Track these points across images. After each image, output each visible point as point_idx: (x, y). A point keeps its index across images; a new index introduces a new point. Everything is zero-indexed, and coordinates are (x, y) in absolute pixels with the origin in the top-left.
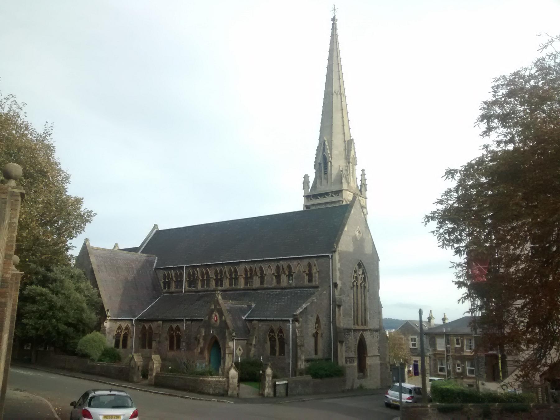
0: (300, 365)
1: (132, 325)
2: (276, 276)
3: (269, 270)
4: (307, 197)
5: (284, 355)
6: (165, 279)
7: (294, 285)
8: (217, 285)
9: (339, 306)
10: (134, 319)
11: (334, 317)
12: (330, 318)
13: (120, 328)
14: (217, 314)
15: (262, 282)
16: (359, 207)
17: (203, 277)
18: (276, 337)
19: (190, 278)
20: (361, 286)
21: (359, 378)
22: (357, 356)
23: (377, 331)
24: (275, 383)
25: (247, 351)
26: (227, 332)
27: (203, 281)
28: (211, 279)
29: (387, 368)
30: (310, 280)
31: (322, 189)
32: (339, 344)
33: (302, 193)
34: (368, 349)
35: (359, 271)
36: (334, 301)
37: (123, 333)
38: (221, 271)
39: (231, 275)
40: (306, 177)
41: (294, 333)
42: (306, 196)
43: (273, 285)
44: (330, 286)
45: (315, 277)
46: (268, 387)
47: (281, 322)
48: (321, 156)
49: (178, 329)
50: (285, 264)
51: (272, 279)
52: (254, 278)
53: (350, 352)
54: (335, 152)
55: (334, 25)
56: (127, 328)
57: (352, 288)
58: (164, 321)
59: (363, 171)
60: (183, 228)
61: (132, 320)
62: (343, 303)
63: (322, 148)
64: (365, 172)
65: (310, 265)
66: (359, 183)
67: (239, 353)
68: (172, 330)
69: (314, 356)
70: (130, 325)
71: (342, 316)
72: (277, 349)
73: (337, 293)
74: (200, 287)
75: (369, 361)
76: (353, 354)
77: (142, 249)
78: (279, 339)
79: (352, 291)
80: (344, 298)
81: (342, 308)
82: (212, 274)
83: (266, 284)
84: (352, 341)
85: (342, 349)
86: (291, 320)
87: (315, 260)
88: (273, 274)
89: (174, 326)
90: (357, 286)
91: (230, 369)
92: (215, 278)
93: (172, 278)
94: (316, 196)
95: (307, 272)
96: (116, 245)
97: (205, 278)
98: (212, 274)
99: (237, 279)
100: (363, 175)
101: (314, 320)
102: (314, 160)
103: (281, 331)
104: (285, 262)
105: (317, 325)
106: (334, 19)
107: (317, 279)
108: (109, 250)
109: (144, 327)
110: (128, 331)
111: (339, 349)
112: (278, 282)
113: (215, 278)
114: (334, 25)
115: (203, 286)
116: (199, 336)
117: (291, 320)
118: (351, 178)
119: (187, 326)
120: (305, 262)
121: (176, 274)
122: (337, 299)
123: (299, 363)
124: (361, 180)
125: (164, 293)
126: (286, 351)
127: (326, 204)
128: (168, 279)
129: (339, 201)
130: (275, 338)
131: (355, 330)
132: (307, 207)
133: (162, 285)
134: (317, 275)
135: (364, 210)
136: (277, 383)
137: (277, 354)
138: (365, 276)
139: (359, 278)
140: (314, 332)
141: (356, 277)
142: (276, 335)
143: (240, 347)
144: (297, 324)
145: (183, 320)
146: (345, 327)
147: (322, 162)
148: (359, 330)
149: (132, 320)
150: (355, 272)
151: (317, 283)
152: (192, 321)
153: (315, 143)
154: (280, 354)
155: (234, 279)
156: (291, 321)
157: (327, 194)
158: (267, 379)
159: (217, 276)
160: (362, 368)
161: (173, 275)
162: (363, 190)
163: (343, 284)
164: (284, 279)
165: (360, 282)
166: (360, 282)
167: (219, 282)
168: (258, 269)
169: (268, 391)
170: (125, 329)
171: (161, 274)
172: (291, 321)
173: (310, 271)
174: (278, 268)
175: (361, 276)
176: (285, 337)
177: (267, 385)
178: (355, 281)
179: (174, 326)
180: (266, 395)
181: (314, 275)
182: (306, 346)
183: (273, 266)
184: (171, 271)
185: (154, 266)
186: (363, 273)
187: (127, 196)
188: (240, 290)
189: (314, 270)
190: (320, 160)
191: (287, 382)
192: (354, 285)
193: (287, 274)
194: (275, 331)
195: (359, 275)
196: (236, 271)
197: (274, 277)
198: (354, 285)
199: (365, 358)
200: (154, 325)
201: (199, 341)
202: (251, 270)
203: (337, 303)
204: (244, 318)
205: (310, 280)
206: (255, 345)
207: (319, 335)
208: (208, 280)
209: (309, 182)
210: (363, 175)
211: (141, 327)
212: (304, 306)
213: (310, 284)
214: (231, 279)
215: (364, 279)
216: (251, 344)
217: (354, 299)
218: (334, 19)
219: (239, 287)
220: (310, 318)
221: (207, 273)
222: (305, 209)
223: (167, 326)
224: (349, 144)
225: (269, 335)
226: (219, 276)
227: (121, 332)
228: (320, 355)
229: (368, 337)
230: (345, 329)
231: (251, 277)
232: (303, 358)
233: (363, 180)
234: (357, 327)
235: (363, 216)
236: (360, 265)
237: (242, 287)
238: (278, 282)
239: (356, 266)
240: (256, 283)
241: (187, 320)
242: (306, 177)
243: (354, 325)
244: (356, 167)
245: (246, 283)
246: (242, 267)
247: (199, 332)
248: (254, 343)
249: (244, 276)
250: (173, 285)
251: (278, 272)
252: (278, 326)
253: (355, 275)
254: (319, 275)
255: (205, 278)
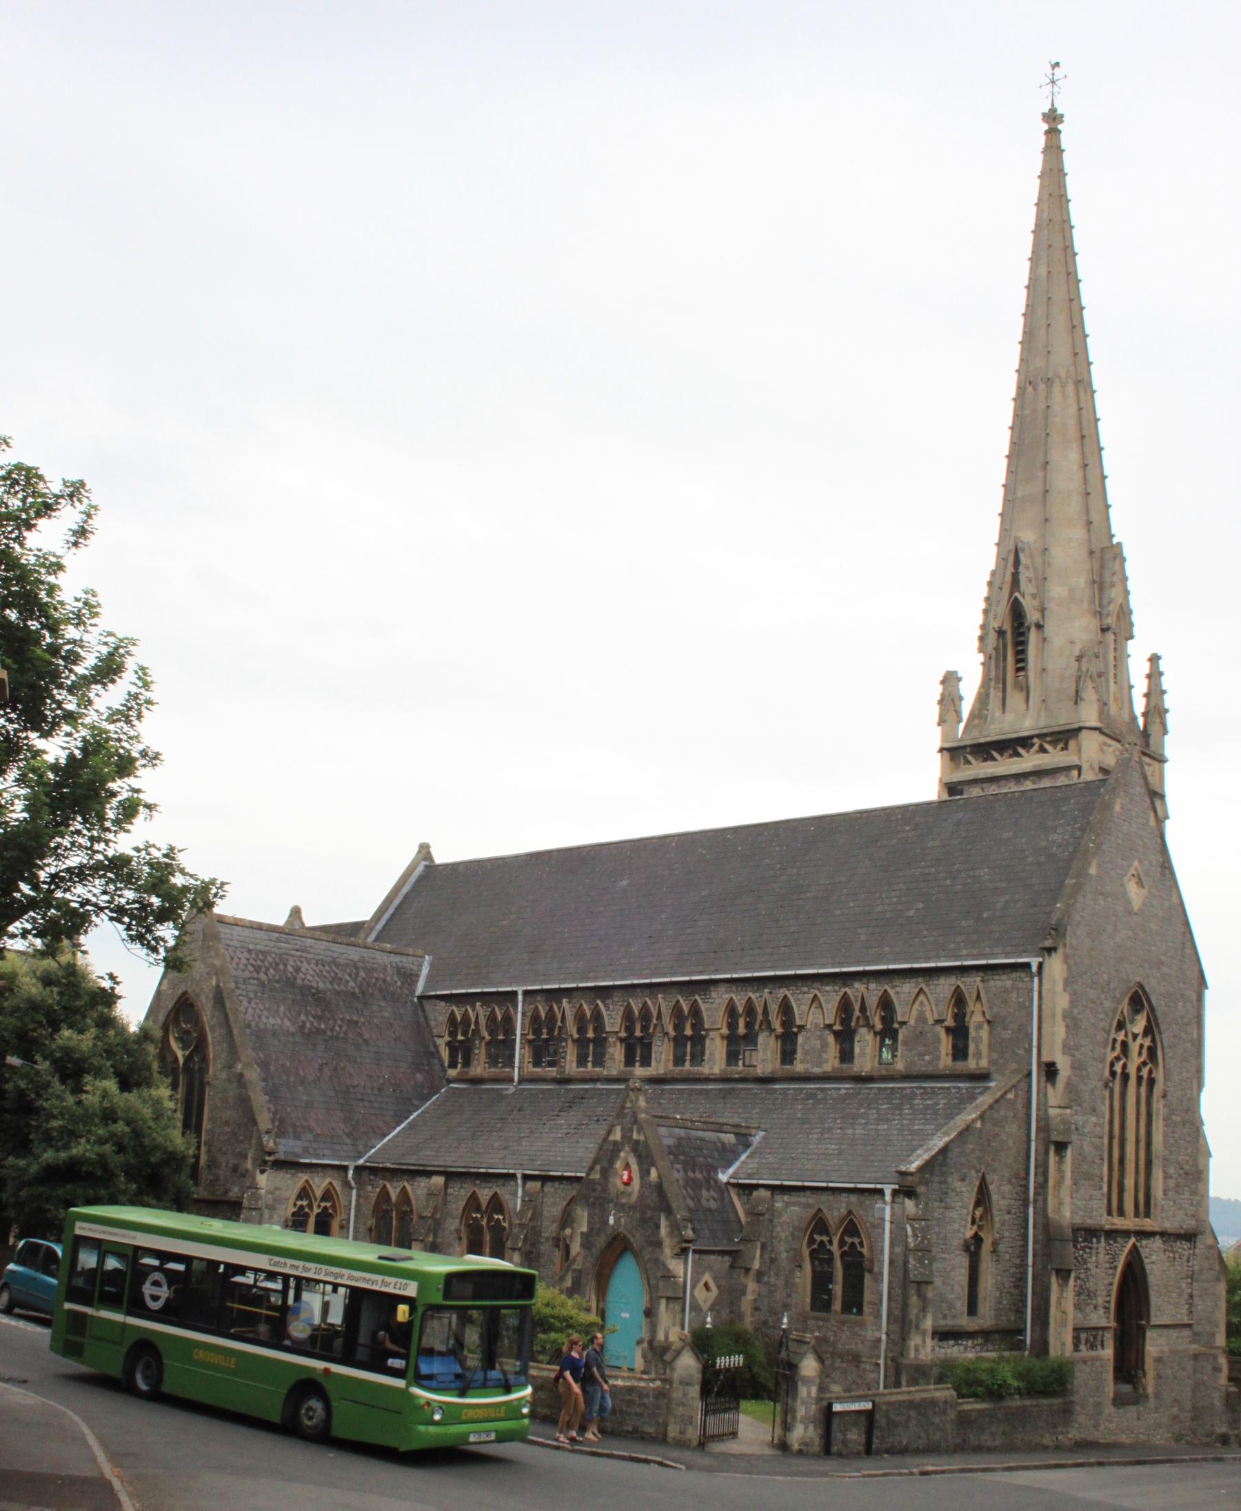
0: (917, 1350)
1: (346, 1184)
2: (837, 1034)
3: (815, 1013)
4: (954, 753)
5: (860, 1312)
6: (453, 1034)
7: (900, 1066)
8: (629, 1061)
9: (1061, 1147)
10: (351, 1165)
11: (1042, 1187)
12: (1026, 1187)
13: (304, 1193)
14: (634, 1166)
15: (788, 1056)
16: (1139, 790)
17: (582, 1029)
18: (835, 1248)
19: (537, 1032)
20: (1139, 1078)
21: (1119, 1401)
22: (1113, 1324)
23: (1189, 1237)
24: (830, 1405)
25: (730, 1296)
26: (664, 1223)
27: (582, 1043)
28: (611, 1040)
29: (1217, 1369)
30: (960, 1052)
31: (1019, 719)
32: (1054, 1279)
33: (935, 738)
34: (1155, 1299)
35: (1132, 1021)
36: (1044, 1127)
37: (316, 1211)
38: (645, 1009)
39: (678, 1027)
40: (951, 680)
41: (898, 1236)
42: (949, 750)
43: (827, 1068)
44: (1029, 1075)
45: (978, 1040)
46: (805, 1421)
47: (853, 1198)
48: (1003, 608)
49: (496, 1204)
50: (872, 992)
51: (825, 1045)
52: (761, 1039)
53: (1089, 1309)
54: (1057, 590)
55: (1053, 133)
56: (328, 1195)
57: (1106, 1086)
58: (450, 1176)
59: (1154, 659)
60: (559, 851)
61: (345, 1168)
62: (1074, 1138)
63: (1008, 578)
64: (1163, 665)
65: (959, 1000)
66: (1139, 706)
67: (705, 1298)
68: (478, 1209)
69: (965, 1322)
70: (338, 1186)
71: (1068, 1181)
72: (837, 1288)
73: (1052, 1101)
74: (570, 1065)
75: (1154, 1345)
76: (1102, 1318)
77: (379, 927)
78: (843, 1255)
79: (1107, 1093)
80: (1080, 1119)
81: (1069, 1152)
82: (613, 1020)
83: (802, 1062)
84: (1102, 1271)
85: (1064, 1304)
86: (888, 1190)
87: (976, 980)
88: (829, 1027)
89: (484, 1194)
90: (1125, 1077)
91: (678, 1353)
92: (623, 1034)
93: (476, 1032)
94: (984, 750)
95: (950, 1022)
96: (296, 912)
97: (591, 1035)
98: (613, 1020)
99: (699, 1040)
100: (1154, 676)
101: (968, 1193)
102: (980, 619)
103: (851, 1228)
104: (872, 986)
105: (978, 1213)
106: (1053, 118)
107: (984, 1048)
108: (272, 929)
109: (384, 1194)
110: (334, 1207)
111: (1053, 1298)
112: (846, 1055)
113: (623, 1034)
114: (1053, 133)
115: (582, 1061)
116: (568, 1231)
117: (888, 1190)
118: (1112, 686)
119: (529, 1200)
120: (945, 987)
121: (492, 1018)
122: (1054, 1123)
123: (914, 1340)
124: (1147, 695)
125: (449, 1081)
126: (868, 1296)
127: (1019, 777)
128: (465, 1033)
129: (1068, 769)
130: (830, 1253)
131: (1112, 1234)
132: (952, 788)
133: (445, 1054)
134: (984, 1033)
135: (1158, 804)
136: (837, 1407)
137: (837, 1305)
138: (1153, 1041)
139: (1134, 1047)
140: (969, 1233)
141: (1124, 1045)
142: (836, 1241)
143: (707, 1277)
144: (909, 1204)
145: (513, 1176)
146: (1078, 1220)
147: (1007, 627)
148: (1126, 1234)
149: (345, 1168)
150: (1121, 1026)
151: (984, 1063)
152: (545, 1179)
153: (981, 558)
154: (846, 1308)
155: (690, 1042)
156: (888, 1193)
157: (1025, 742)
158: (803, 1391)
159: (630, 1030)
160: (1128, 1367)
161: (483, 1021)
162: (1154, 730)
163: (1077, 1066)
164: (865, 1043)
165: (1135, 1061)
166: (1135, 1061)
167: (638, 1050)
168: (774, 1008)
169: (801, 1433)
170: (324, 1199)
171: (439, 1015)
172: (888, 1193)
173: (960, 1017)
174: (845, 1006)
175: (1139, 1040)
176: (865, 1251)
177: (801, 1412)
178: (1118, 1058)
179: (484, 1194)
180: (796, 1447)
181: (972, 1033)
182: (937, 1281)
183: (831, 998)
184: (559, 1003)
185: (420, 989)
186: (1148, 1031)
187: (285, 781)
188: (707, 1080)
189: (975, 1018)
190: (1002, 618)
191: (869, 1406)
192: (1113, 1074)
193: (879, 1026)
194: (832, 1229)
195: (1135, 1036)
196: (696, 1012)
197: (831, 1039)
198: (1113, 1074)
199: (1142, 1331)
200: (418, 1190)
201: (567, 1249)
202: (750, 1009)
203: (1056, 1137)
204: (723, 1177)
205: (960, 1052)
206: (759, 1274)
207: (986, 1247)
208: (600, 1043)
209: (961, 698)
210: (1154, 676)
211: (373, 1192)
212: (939, 1142)
213: (960, 1066)
214: (679, 1041)
215: (1152, 1052)
216: (747, 1270)
217: (1111, 1122)
218: (1053, 118)
219: (705, 1070)
220: (958, 1185)
221: (597, 1016)
222: (946, 797)
223: (460, 1193)
224: (1106, 562)
225: (811, 1241)
226: (638, 1027)
227: (310, 1206)
228: (986, 1317)
229: (1155, 1257)
230: (1076, 1230)
231: (750, 1038)
232: (928, 1324)
233: (1155, 693)
234: (1119, 1223)
235: (1152, 822)
236: (1138, 1001)
237: (716, 1070)
238: (846, 1055)
239: (1125, 1006)
240: (765, 1055)
241: (526, 1178)
242: (951, 680)
243: (1109, 1213)
244: (1131, 646)
245: (732, 1057)
246: (720, 997)
247: (566, 1219)
248: (756, 1265)
249: (725, 1031)
250: (480, 1053)
251: (845, 1021)
252: (844, 1211)
253: (1121, 1036)
254: (991, 1033)
255: (591, 1035)
